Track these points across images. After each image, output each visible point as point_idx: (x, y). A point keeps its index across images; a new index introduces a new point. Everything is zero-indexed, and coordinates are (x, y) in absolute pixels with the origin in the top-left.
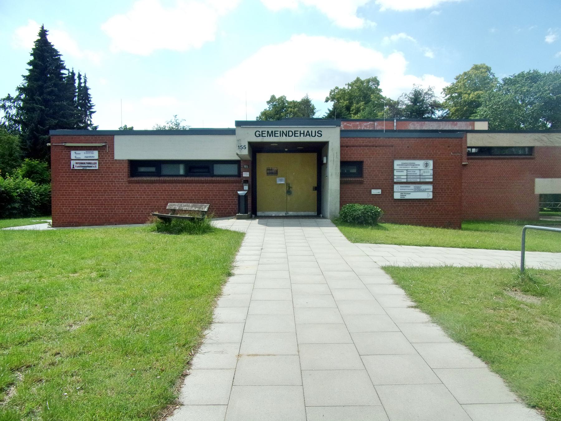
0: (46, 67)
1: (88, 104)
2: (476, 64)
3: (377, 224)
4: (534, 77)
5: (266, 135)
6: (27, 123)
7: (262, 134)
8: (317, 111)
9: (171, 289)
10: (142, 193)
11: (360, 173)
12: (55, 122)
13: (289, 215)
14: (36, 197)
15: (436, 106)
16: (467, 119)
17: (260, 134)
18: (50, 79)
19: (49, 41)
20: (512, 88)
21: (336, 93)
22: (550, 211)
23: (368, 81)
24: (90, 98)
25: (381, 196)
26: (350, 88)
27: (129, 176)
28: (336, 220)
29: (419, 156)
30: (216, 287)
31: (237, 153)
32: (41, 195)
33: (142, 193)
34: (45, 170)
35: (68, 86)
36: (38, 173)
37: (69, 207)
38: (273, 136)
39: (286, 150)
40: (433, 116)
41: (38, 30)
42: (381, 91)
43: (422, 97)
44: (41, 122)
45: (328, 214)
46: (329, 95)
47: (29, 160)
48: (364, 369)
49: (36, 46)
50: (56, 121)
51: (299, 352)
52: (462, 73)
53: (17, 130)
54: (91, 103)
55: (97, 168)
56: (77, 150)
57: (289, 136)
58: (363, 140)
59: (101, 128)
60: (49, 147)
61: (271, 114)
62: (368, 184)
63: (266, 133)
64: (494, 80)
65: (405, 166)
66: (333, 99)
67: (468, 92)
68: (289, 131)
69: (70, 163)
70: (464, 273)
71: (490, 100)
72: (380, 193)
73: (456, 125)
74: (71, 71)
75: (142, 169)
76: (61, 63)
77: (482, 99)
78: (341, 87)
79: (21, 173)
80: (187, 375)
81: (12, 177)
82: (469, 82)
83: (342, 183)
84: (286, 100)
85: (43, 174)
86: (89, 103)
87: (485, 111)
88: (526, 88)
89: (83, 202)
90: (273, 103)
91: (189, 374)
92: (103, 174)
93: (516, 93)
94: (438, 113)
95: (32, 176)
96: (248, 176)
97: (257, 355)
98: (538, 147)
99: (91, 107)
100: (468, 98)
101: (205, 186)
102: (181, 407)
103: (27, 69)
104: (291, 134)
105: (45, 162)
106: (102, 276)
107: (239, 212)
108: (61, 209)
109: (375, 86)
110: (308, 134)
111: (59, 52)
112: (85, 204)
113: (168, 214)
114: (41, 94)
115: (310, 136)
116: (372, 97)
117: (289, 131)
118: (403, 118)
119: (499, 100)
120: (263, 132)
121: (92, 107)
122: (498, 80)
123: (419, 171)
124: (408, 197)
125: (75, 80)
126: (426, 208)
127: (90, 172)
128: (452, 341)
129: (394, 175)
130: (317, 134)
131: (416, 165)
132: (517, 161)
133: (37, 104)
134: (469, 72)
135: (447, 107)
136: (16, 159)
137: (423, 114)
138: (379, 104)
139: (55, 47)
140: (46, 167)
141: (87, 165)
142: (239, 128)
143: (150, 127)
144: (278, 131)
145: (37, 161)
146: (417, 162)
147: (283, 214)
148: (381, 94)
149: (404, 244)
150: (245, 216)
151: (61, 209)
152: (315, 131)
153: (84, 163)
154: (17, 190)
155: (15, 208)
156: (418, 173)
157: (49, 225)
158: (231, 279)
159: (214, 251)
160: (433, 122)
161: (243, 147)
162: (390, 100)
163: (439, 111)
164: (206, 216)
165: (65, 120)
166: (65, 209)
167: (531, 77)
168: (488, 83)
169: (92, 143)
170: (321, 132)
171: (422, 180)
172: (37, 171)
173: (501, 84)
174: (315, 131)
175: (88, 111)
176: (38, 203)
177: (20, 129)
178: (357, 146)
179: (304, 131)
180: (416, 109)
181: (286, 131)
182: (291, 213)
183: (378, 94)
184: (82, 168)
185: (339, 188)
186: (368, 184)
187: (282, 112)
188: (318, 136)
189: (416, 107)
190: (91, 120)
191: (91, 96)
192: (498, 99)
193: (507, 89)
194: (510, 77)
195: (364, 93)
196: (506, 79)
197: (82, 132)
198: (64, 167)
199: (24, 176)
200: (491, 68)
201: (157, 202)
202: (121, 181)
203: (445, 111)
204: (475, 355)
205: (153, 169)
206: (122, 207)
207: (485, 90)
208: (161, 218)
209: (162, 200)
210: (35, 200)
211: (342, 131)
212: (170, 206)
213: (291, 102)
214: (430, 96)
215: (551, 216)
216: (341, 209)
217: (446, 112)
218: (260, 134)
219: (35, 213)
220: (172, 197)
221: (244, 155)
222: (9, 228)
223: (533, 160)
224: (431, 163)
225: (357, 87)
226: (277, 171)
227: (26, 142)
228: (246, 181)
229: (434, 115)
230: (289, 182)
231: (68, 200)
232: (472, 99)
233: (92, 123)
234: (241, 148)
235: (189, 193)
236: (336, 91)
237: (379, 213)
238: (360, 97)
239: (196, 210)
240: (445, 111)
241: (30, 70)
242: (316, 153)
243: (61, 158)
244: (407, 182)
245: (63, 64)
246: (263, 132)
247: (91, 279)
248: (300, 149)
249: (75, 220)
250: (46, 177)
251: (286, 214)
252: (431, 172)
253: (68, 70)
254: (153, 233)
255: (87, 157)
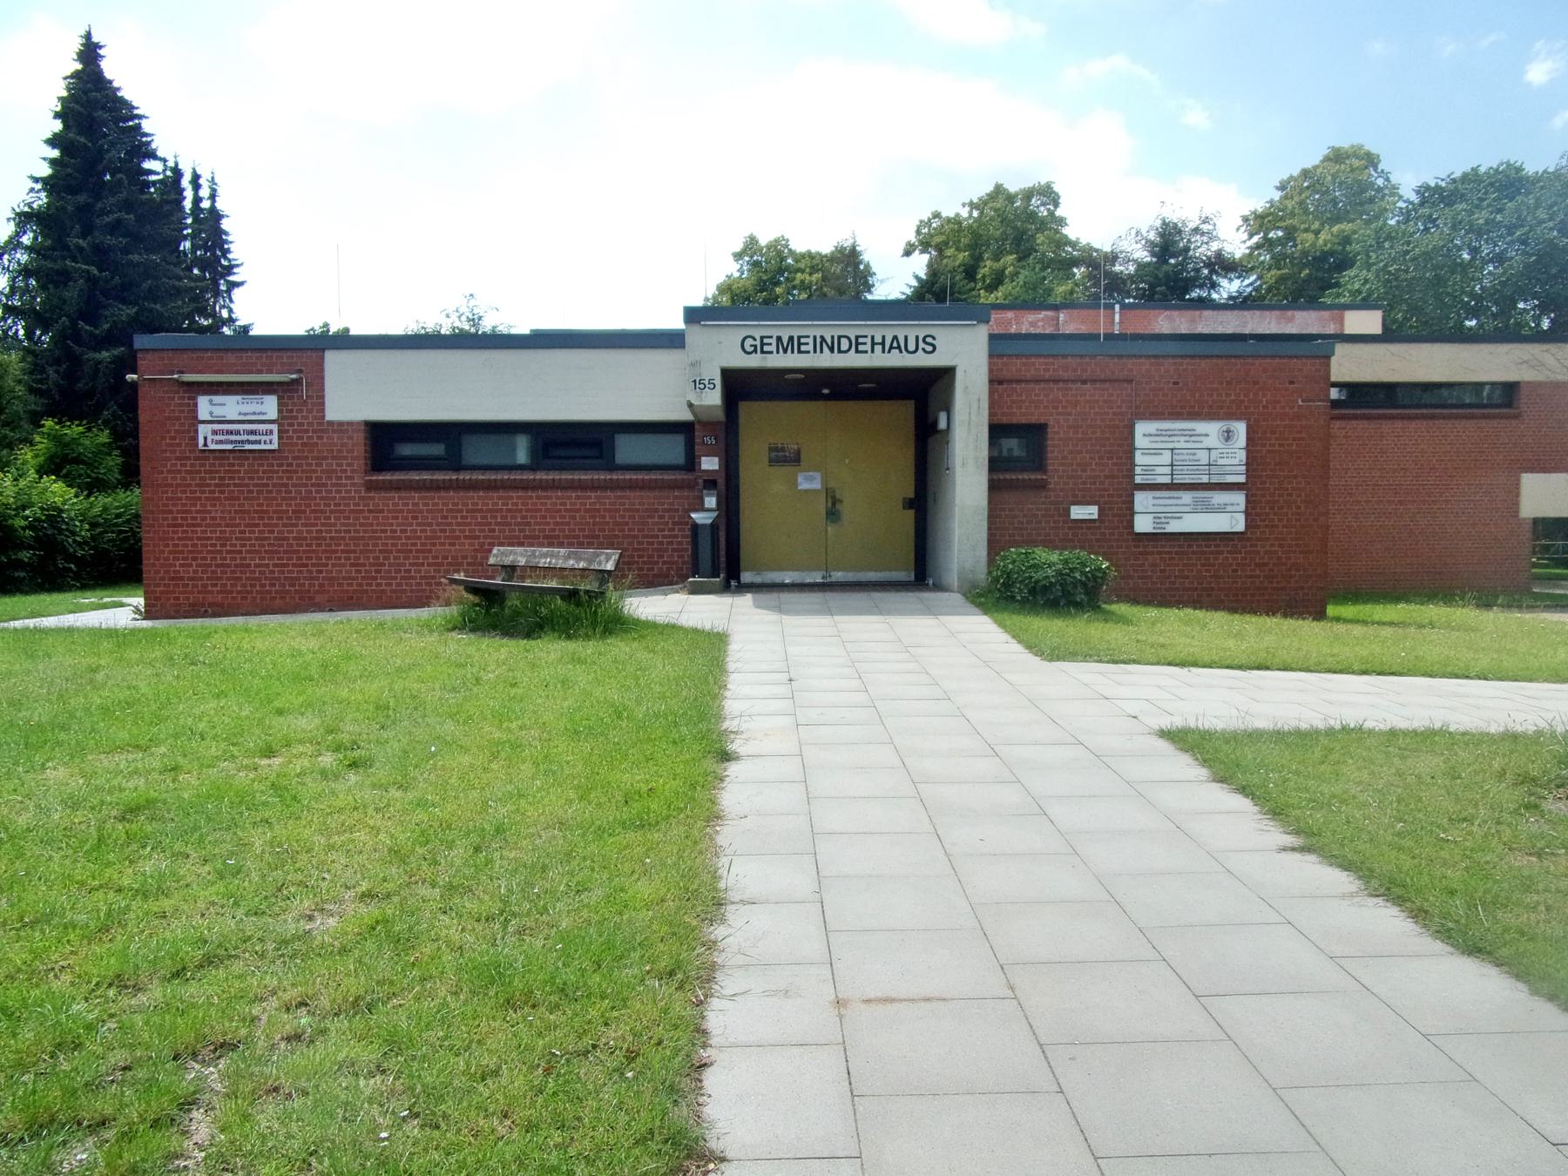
0: (101, 152)
1: (223, 261)
2: (1337, 146)
3: (1099, 607)
4: (1508, 182)
5: (773, 348)
6: (47, 315)
7: (762, 344)
8: (882, 281)
9: (571, 802)
10: (407, 519)
11: (1037, 460)
12: (128, 311)
13: (833, 579)
14: (81, 530)
15: (1224, 265)
16: (1313, 303)
17: (755, 346)
18: (115, 187)
19: (108, 75)
20: (1444, 216)
21: (934, 229)
22: (1547, 566)
23: (1028, 194)
24: (227, 242)
25: (1097, 524)
26: (975, 214)
27: (369, 468)
28: (980, 595)
29: (1206, 410)
30: (699, 794)
31: (689, 401)
32: (93, 525)
33: (407, 519)
34: (100, 452)
35: (167, 208)
36: (83, 462)
37: (195, 559)
38: (793, 352)
39: (826, 391)
40: (1215, 296)
41: (76, 45)
42: (1066, 224)
43: (1182, 239)
44: (90, 313)
45: (953, 578)
46: (914, 234)
47: (56, 423)
48: (1223, 1036)
49: (69, 89)
50: (133, 311)
51: (1012, 988)
52: (1296, 173)
53: (12, 337)
54: (230, 256)
55: (275, 446)
56: (216, 393)
57: (840, 351)
58: (1046, 364)
59: (262, 327)
60: (134, 385)
61: (745, 291)
62: (1061, 490)
63: (774, 341)
64: (1387, 192)
65: (1167, 439)
66: (925, 245)
67: (1313, 227)
68: (839, 337)
69: (196, 431)
70: (1403, 746)
71: (1380, 246)
72: (1096, 517)
73: (1291, 320)
74: (171, 164)
75: (406, 450)
76: (144, 139)
77: (1355, 247)
78: (948, 212)
79: (33, 462)
80: (705, 1065)
81: (8, 472)
82: (1317, 196)
83: (994, 487)
84: (790, 250)
85: (96, 464)
86: (226, 258)
87: (1366, 281)
88: (1485, 214)
89: (235, 545)
90: (752, 257)
91: (712, 1064)
92: (291, 465)
93: (1454, 227)
94: (1229, 287)
95: (64, 471)
96: (716, 467)
97: (891, 1000)
98: (1529, 383)
99: (229, 270)
100: (1313, 245)
101: (590, 497)
102: (723, 1166)
103: (44, 159)
104: (845, 345)
105: (102, 430)
106: (354, 765)
107: (696, 571)
108: (171, 565)
109: (1048, 210)
110: (896, 345)
111: (137, 108)
112: (241, 552)
113: (494, 579)
114: (87, 231)
115: (901, 352)
116: (1038, 241)
117: (839, 337)
118: (1127, 301)
119: (1405, 248)
120: (765, 341)
121: (235, 270)
122: (1401, 192)
123: (1206, 452)
124: (1175, 527)
125: (184, 190)
126: (1227, 558)
127: (254, 459)
128: (1450, 949)
129: (1133, 465)
130: (921, 345)
131: (1199, 435)
132: (1470, 424)
133: (74, 260)
134: (1315, 168)
135: (1252, 269)
136: (12, 422)
137: (1187, 290)
138: (1060, 261)
139: (125, 93)
140: (104, 445)
141: (245, 437)
142: (696, 328)
143: (523, 329)
144: (808, 337)
145: (77, 426)
146: (1201, 427)
147: (817, 577)
148: (1065, 231)
149: (1195, 664)
150: (713, 583)
151: (171, 565)
152: (917, 337)
153: (238, 433)
154: (24, 510)
155: (19, 564)
156: (1203, 457)
157: (136, 613)
158: (733, 769)
159: (658, 689)
160: (1225, 312)
161: (707, 383)
162: (1092, 249)
163: (1231, 280)
164: (611, 585)
165: (158, 307)
166: (181, 565)
167: (1500, 181)
168: (1371, 200)
169: (260, 372)
170: (934, 338)
171: (1215, 480)
172: (78, 456)
173: (1412, 203)
174: (917, 337)
175: (222, 282)
176: (84, 550)
177: (21, 332)
178: (1027, 381)
179: (884, 337)
180: (1167, 274)
181: (833, 337)
182: (838, 576)
183: (1057, 232)
184: (229, 447)
185: (985, 503)
186: (1061, 490)
187: (778, 283)
188: (923, 349)
189: (1165, 268)
190: (232, 306)
191: (230, 238)
192: (1403, 244)
193: (1431, 216)
194: (1440, 183)
195: (1015, 228)
196: (1427, 188)
197: (207, 340)
198: (179, 445)
199: (42, 471)
200: (1378, 156)
201: (450, 544)
202: (346, 485)
203: (1247, 282)
204: (1535, 992)
205: (437, 449)
206: (349, 559)
207: (1362, 219)
208: (474, 589)
209: (466, 537)
210: (78, 539)
211: (993, 338)
212: (500, 555)
213: (803, 256)
214: (1205, 239)
215: (1558, 579)
216: (991, 561)
217: (1251, 284)
218: (755, 346)
219: (77, 576)
220: (494, 531)
221: (710, 407)
222: (18, 624)
223: (1514, 422)
224: (1240, 428)
225: (996, 210)
226: (798, 453)
227: (43, 371)
228: (710, 483)
229: (1217, 292)
230: (831, 485)
231: (208, 539)
232: (1326, 245)
233: (234, 316)
234: (702, 386)
235: (545, 517)
236: (934, 225)
237: (1105, 572)
238: (1004, 240)
239: (581, 566)
240: (1247, 282)
241: (53, 162)
242: (913, 402)
243: (169, 418)
244: (1172, 484)
245: (149, 143)
246: (765, 341)
247: (324, 774)
248: (868, 389)
249: (210, 598)
250: (104, 474)
251: (823, 578)
252: (1242, 455)
253: (165, 161)
254: (453, 634)
255: (245, 414)
